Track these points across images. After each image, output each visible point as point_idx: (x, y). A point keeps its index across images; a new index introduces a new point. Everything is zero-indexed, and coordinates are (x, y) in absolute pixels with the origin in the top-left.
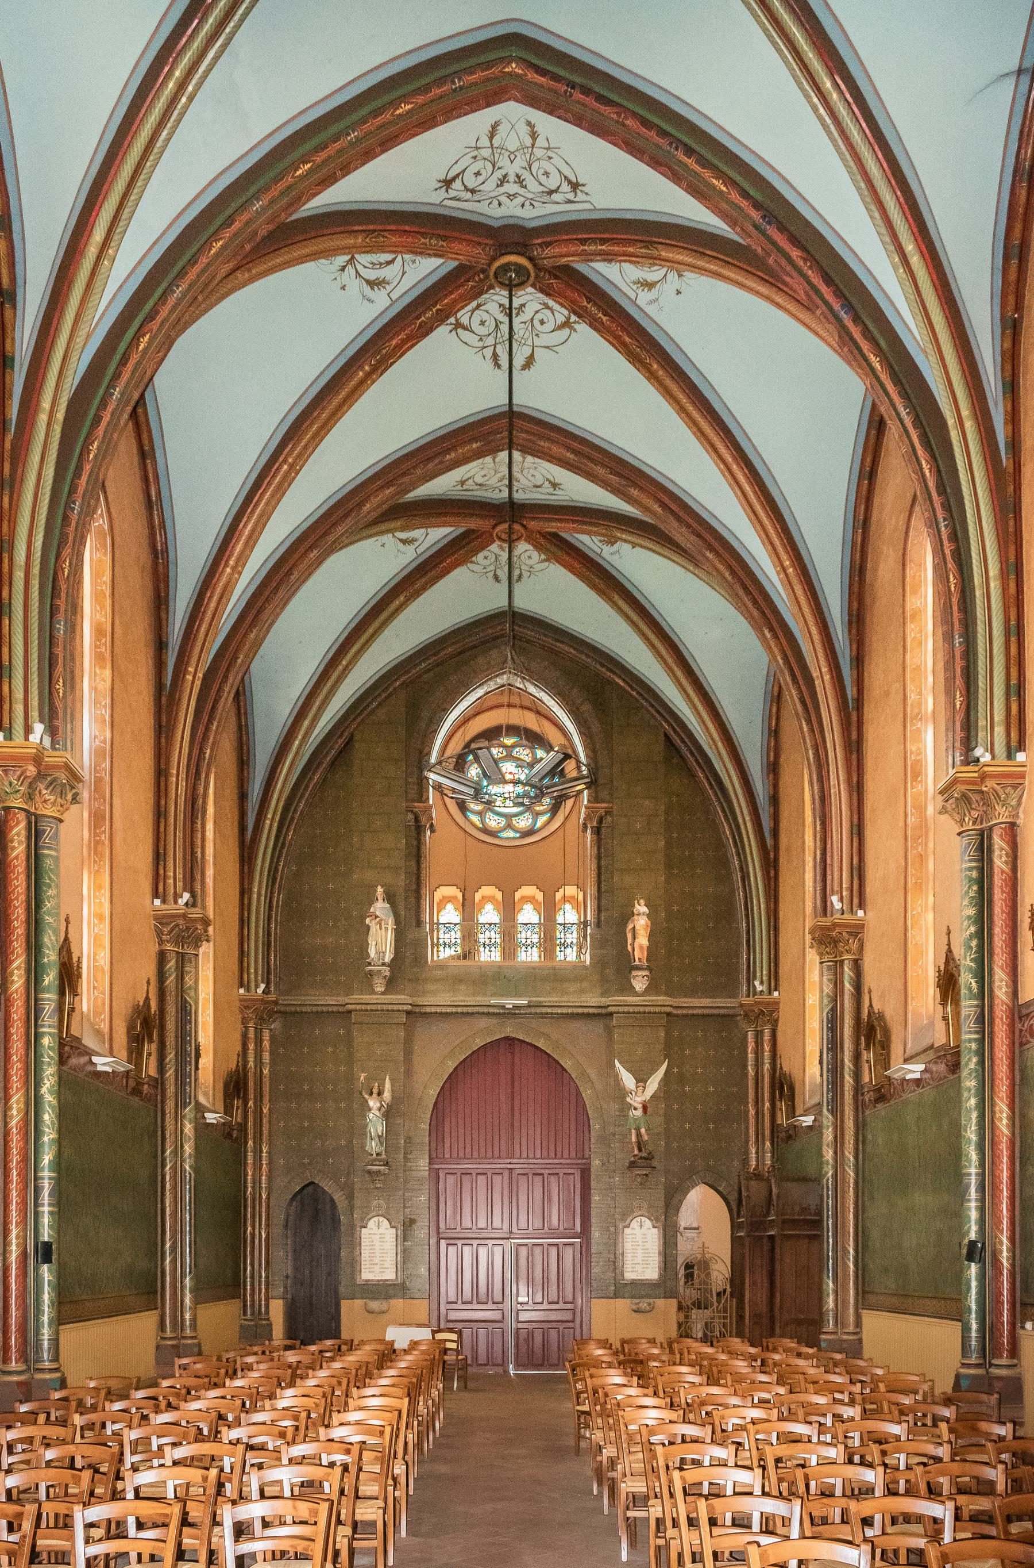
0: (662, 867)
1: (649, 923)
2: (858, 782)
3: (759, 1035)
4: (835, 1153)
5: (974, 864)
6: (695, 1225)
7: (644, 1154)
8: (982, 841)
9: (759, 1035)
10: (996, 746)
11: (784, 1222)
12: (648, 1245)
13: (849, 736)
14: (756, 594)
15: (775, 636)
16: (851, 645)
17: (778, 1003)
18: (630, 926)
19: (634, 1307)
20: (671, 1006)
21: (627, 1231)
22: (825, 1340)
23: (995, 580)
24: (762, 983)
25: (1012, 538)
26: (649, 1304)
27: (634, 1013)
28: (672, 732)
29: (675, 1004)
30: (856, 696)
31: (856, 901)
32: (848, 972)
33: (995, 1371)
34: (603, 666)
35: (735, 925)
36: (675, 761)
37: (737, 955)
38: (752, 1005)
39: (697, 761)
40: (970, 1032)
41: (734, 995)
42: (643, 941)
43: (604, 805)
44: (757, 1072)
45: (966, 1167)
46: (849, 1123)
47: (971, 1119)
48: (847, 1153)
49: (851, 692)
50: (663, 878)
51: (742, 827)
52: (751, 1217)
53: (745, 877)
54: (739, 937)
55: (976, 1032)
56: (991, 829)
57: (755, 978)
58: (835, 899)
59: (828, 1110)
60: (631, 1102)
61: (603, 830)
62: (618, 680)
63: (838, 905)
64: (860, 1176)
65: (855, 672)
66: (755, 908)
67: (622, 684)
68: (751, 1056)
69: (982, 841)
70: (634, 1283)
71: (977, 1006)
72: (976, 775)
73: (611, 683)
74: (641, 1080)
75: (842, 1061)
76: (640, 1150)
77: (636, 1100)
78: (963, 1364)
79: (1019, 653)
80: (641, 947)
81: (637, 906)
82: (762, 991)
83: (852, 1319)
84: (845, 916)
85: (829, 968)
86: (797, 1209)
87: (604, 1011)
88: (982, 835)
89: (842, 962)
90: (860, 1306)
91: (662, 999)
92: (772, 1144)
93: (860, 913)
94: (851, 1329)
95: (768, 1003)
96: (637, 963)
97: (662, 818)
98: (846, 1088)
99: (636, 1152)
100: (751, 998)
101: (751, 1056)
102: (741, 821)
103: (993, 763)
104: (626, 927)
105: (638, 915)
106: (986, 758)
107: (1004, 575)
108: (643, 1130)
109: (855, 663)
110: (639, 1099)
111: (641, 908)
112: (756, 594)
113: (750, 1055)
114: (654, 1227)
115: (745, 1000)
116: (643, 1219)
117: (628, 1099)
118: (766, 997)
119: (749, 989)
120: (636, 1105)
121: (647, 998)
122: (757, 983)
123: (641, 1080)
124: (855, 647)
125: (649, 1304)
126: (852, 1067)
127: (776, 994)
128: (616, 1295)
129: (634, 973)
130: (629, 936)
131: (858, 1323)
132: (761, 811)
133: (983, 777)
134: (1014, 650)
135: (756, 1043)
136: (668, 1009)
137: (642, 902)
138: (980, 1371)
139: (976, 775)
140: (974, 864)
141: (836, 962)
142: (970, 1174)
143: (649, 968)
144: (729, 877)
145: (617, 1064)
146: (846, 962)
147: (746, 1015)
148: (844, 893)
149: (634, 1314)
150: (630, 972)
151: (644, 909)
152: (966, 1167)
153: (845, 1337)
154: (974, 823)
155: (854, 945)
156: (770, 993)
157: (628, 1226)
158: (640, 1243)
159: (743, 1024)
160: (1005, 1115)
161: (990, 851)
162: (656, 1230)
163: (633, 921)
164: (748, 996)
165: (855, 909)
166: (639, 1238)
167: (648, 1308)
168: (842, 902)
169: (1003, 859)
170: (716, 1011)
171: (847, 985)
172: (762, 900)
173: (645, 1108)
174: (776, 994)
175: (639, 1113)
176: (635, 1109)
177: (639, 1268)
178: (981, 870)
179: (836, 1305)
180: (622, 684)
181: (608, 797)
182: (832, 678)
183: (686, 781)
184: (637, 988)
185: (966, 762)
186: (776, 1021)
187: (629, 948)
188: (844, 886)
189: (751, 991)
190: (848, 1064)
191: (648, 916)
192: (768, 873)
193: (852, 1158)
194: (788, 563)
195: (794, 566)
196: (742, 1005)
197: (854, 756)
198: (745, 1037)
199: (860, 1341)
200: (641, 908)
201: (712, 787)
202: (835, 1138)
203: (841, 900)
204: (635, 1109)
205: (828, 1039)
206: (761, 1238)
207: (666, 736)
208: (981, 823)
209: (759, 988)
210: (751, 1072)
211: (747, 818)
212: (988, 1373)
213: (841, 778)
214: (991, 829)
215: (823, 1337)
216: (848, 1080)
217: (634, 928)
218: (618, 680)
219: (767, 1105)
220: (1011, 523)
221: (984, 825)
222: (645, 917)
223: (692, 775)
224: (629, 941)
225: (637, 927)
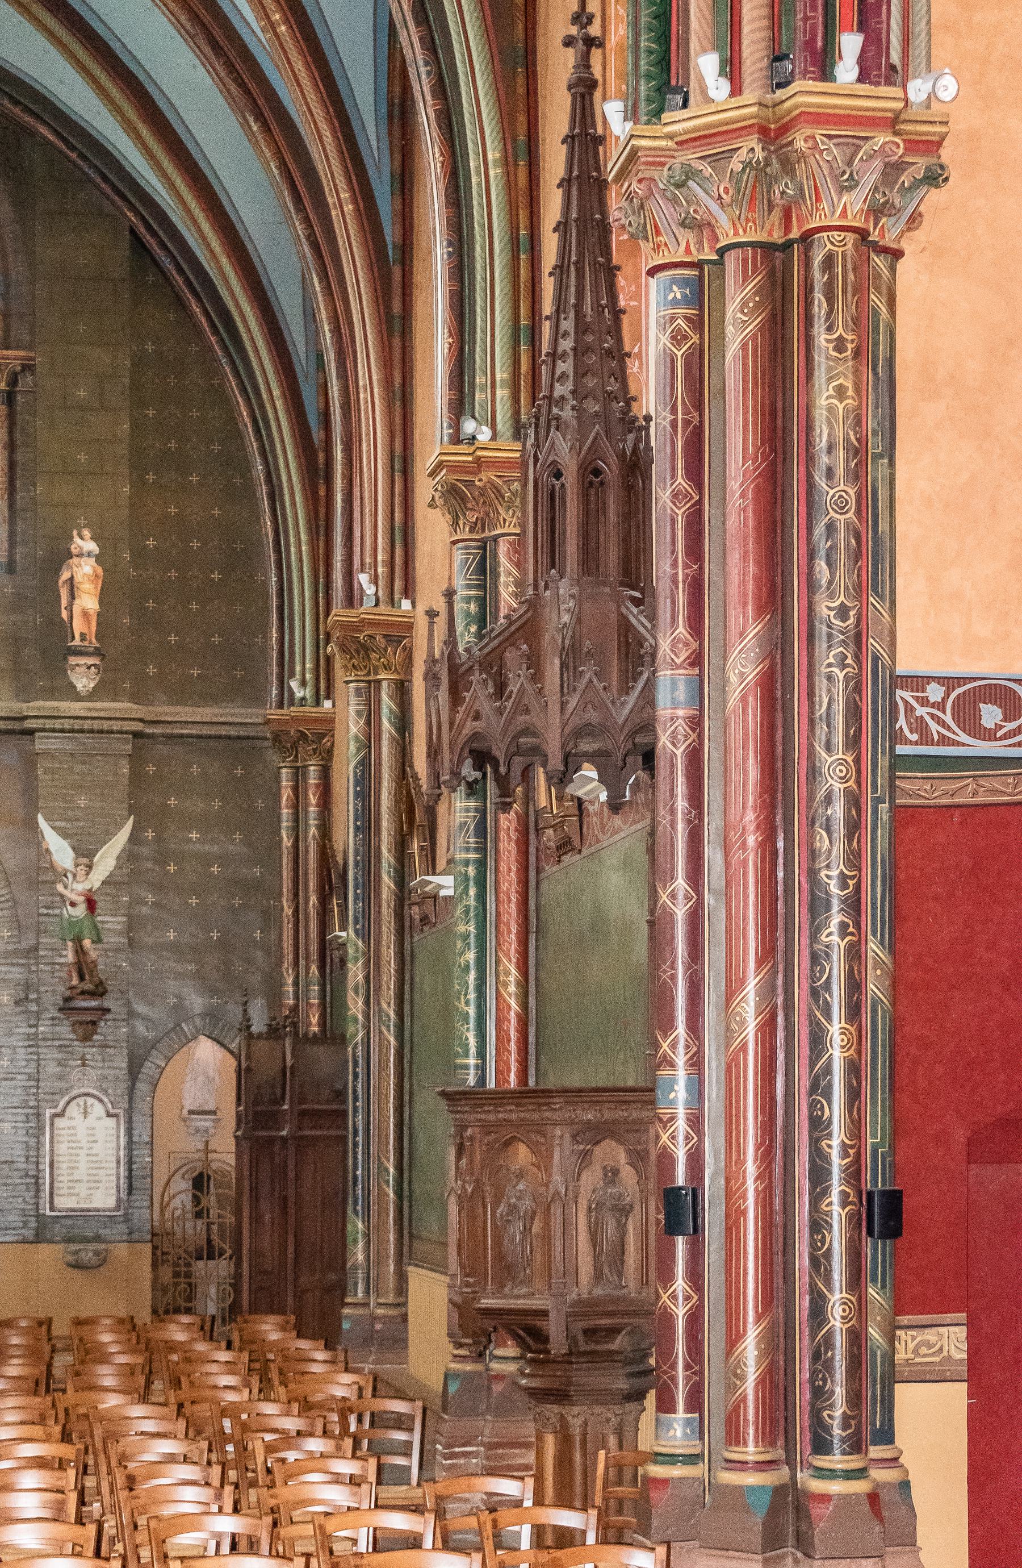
0: (126, 471)
1: (100, 570)
2: (404, 385)
3: (299, 775)
4: (367, 1003)
5: (473, 592)
6: (211, 1107)
7: (88, 986)
8: (484, 558)
9: (299, 775)
10: (499, 417)
11: (303, 1113)
12: (97, 1148)
13: (388, 308)
14: (232, 54)
15: (266, 128)
16: (392, 155)
17: (332, 721)
18: (65, 576)
19: (70, 1258)
20: (141, 720)
21: (59, 1122)
22: (348, 1317)
23: (495, 166)
24: (303, 683)
25: (521, 104)
26: (97, 1253)
27: (72, 731)
28: (142, 229)
29: (148, 718)
30: (399, 240)
31: (398, 584)
32: (387, 703)
33: (495, 1366)
34: (16, 102)
35: (260, 578)
36: (150, 279)
37: (264, 630)
38: (286, 722)
39: (188, 282)
40: (467, 849)
41: (258, 699)
42: (88, 601)
43: (21, 353)
44: (297, 840)
45: (457, 1055)
46: (389, 953)
47: (467, 983)
48: (384, 1005)
49: (390, 233)
50: (127, 489)
51: (268, 407)
52: (255, 1103)
53: (274, 495)
54: (267, 596)
55: (477, 850)
56: (495, 539)
57: (292, 675)
58: (363, 578)
59: (356, 932)
60: (66, 893)
61: (20, 399)
62: (43, 130)
63: (370, 590)
64: (407, 1044)
65: (399, 201)
66: (293, 550)
67: (51, 137)
68: (286, 812)
69: (484, 558)
70: (73, 1215)
71: (476, 810)
72: (470, 459)
73: (32, 133)
74: (86, 854)
75: (378, 849)
76: (82, 978)
77: (76, 889)
78: (455, 1356)
79: (533, 278)
80: (85, 614)
81: (77, 540)
82: (303, 699)
83: (391, 1283)
84: (383, 608)
85: (358, 692)
86: (325, 1095)
87: (17, 726)
88: (484, 548)
89: (379, 682)
90: (406, 1260)
91: (124, 707)
92: (322, 968)
93: (406, 605)
94: (391, 1299)
95: (316, 720)
96: (77, 642)
97: (126, 381)
98: (384, 895)
99: (75, 982)
100: (285, 711)
101: (286, 812)
102: (265, 396)
103: (493, 445)
104: (59, 577)
105: (80, 555)
106: (484, 435)
107: (507, 162)
108: (87, 943)
109: (397, 186)
110: (80, 887)
111: (85, 543)
112: (232, 54)
113: (285, 811)
114: (109, 1115)
115: (274, 713)
116: (90, 1101)
117: (60, 888)
118: (310, 710)
119: (281, 694)
120: (74, 897)
121: (98, 705)
122: (294, 684)
123: (86, 854)
124: (398, 157)
125: (97, 1253)
126: (392, 860)
127: (328, 704)
128: (39, 1238)
129: (73, 660)
130: (64, 593)
131: (402, 1289)
132: (301, 379)
133: (479, 464)
134: (524, 274)
135: (295, 789)
136: (137, 726)
137: (86, 533)
138: (478, 1367)
139: (470, 459)
140: (473, 592)
141: (369, 682)
142: (467, 1067)
143: (97, 652)
144: (249, 489)
145: (40, 819)
146: (385, 684)
147: (276, 739)
148: (380, 570)
149: (74, 1273)
150: (65, 659)
151: (91, 546)
152: (457, 1055)
153: (380, 1311)
154: (471, 531)
155: (397, 657)
156: (318, 703)
157: (61, 1115)
158: (84, 1144)
159: (273, 758)
160: (512, 979)
161: (496, 575)
162: (111, 1122)
163: (70, 567)
164: (280, 705)
165: (397, 596)
166: (82, 1134)
167: (95, 1261)
168: (376, 584)
169: (510, 590)
170: (223, 731)
171: (386, 724)
172: (304, 537)
173: (91, 904)
174: (328, 704)
175: (80, 911)
176: (73, 904)
177: (82, 1189)
178: (482, 602)
179: (368, 1258)
180: (51, 137)
181: (26, 338)
182: (357, 209)
183: (171, 316)
184: (79, 686)
185: (456, 439)
186: (330, 751)
187: (64, 614)
188: (380, 558)
189: (285, 698)
190: (387, 856)
191: (99, 559)
192: (315, 492)
193: (392, 1015)
194: (277, 16)
195: (287, 22)
196: (268, 722)
197: (397, 341)
198: (278, 779)
199: (404, 1318)
200: (85, 543)
201: (216, 332)
202: (367, 978)
203: (375, 580)
204: (73, 904)
205: (356, 810)
206: (271, 1140)
207: (132, 231)
208: (483, 531)
209: (299, 693)
210: (287, 841)
211: (276, 392)
212: (488, 1370)
213: (375, 377)
214: (495, 539)
215: (346, 1311)
216: (388, 883)
217: (72, 579)
218: (43, 130)
219: (313, 899)
220: (521, 81)
221: (487, 534)
222: (92, 561)
223: (181, 304)
224: (64, 602)
225: (78, 578)
